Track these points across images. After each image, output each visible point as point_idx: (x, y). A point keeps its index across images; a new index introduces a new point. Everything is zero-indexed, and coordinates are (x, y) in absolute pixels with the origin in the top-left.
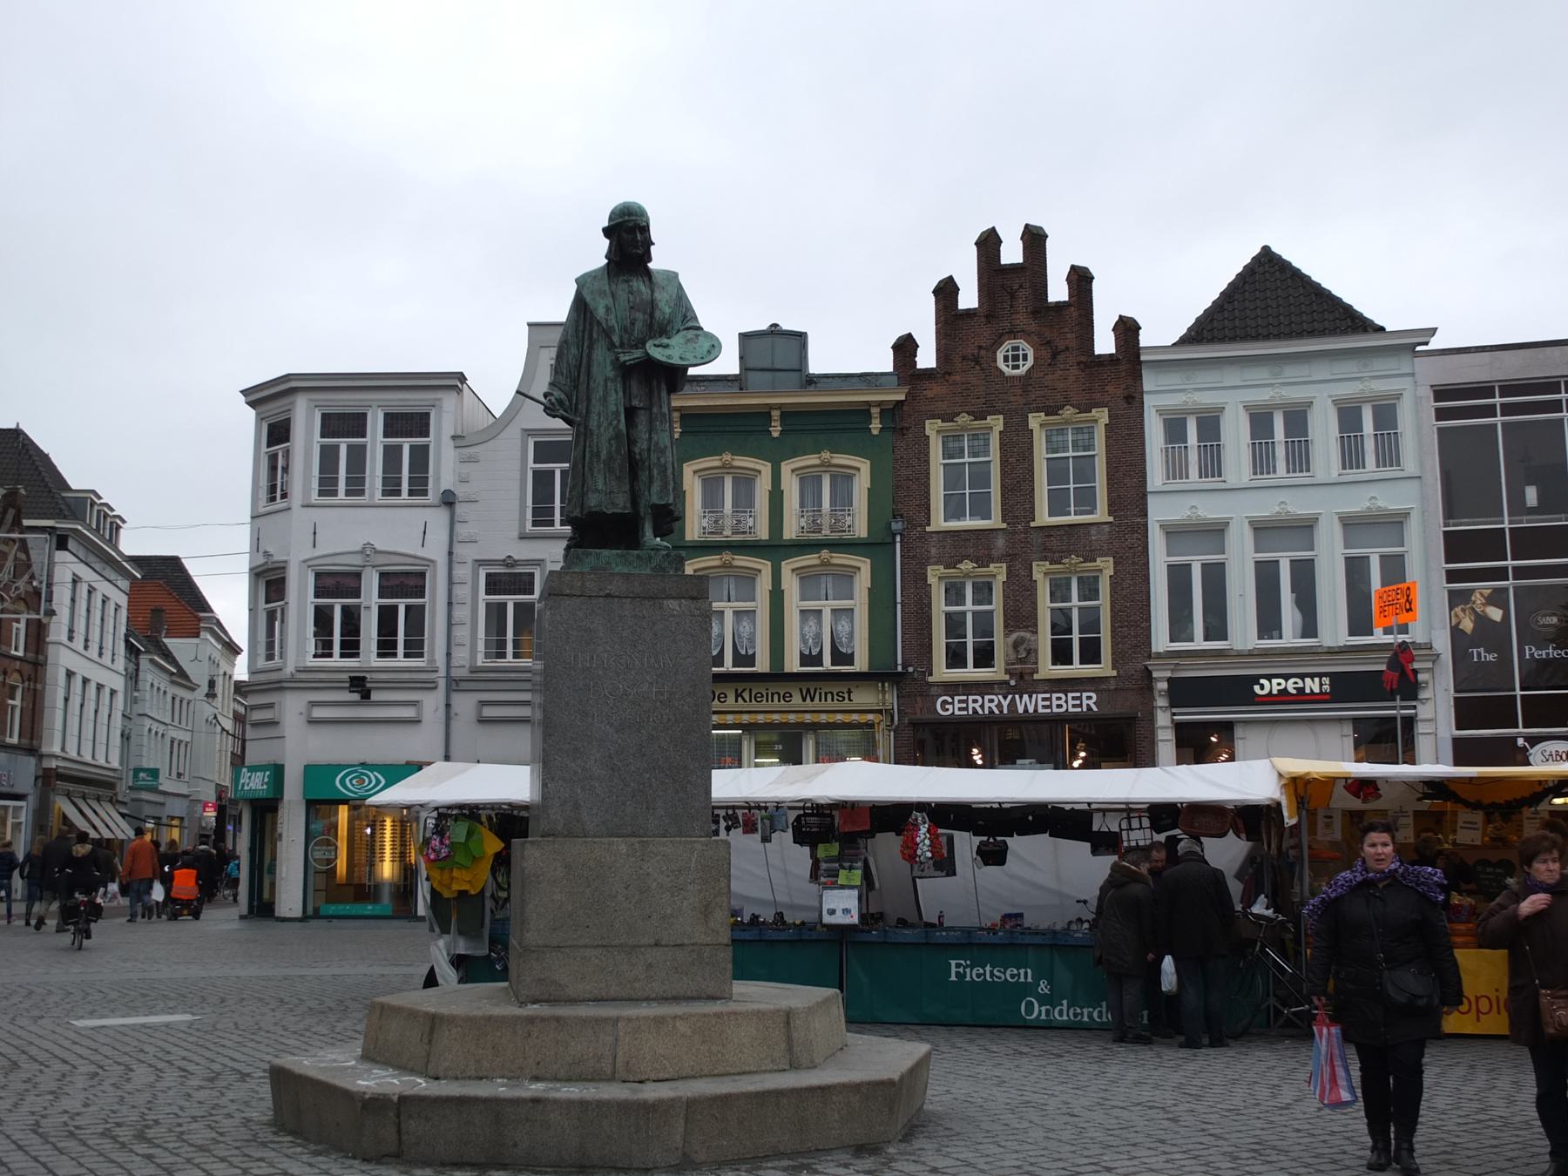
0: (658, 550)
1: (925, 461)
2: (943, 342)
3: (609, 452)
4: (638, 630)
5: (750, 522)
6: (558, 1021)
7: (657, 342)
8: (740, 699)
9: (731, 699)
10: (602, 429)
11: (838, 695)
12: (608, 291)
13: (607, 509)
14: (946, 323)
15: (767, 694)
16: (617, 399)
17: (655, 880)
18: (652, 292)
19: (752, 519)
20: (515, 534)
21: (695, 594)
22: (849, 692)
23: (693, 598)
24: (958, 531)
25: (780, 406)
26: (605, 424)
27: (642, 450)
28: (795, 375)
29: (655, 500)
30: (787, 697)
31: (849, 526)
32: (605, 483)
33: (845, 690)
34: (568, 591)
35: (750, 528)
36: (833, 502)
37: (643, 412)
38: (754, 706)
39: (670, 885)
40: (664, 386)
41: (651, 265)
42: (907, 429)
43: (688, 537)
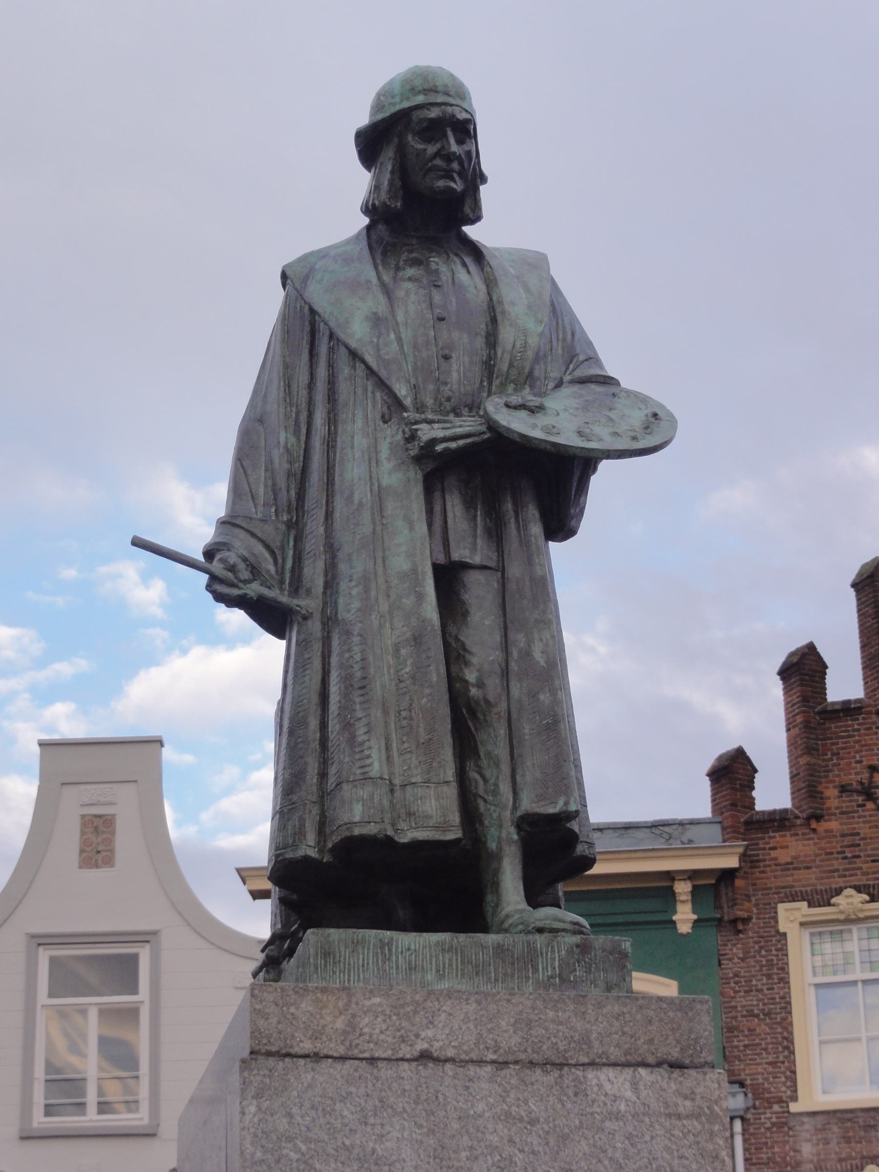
0: (554, 931)
1: (781, 980)
2: (802, 761)
7: (515, 400)
12: (374, 280)
14: (807, 726)
20: (13, 1131)
21: (675, 1054)
23: (676, 1066)
24: (852, 1111)
29: (528, 804)
34: (307, 1046)
40: (532, 512)
42: (746, 921)
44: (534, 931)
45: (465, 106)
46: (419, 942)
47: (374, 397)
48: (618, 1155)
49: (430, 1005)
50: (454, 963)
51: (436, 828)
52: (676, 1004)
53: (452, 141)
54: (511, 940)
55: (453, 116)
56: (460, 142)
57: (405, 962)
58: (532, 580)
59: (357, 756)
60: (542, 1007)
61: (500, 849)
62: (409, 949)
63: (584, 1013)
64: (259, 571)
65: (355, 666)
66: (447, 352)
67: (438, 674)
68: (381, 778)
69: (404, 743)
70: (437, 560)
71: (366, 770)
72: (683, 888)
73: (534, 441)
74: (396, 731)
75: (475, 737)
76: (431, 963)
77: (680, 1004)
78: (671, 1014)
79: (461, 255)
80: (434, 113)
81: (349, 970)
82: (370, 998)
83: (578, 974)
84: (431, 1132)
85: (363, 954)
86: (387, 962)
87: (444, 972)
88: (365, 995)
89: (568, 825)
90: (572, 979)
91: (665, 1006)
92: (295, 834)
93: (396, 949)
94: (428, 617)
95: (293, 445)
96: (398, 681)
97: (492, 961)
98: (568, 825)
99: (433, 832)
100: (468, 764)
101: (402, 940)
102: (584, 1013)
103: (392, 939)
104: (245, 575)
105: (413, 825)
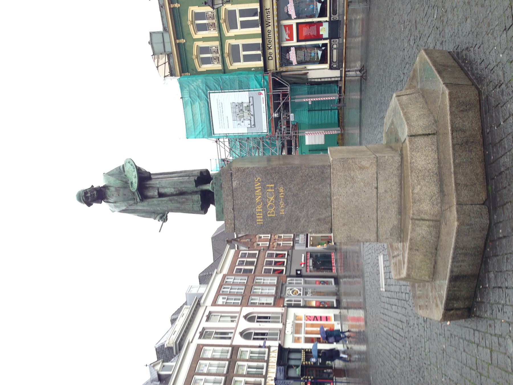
4: (246, 197)
5: (214, 48)
6: (412, 240)
8: (271, 48)
9: (271, 51)
11: (268, 14)
15: (269, 38)
17: (349, 190)
19: (213, 47)
22: (266, 9)
25: (175, 40)
28: (164, 35)
30: (269, 32)
31: (212, 13)
33: (266, 11)
34: (233, 225)
35: (216, 48)
36: (204, 19)
38: (273, 43)
39: (351, 184)
43: (221, 68)
48: (245, 183)
72: (172, 6)
80: (84, 198)
84: (244, 209)
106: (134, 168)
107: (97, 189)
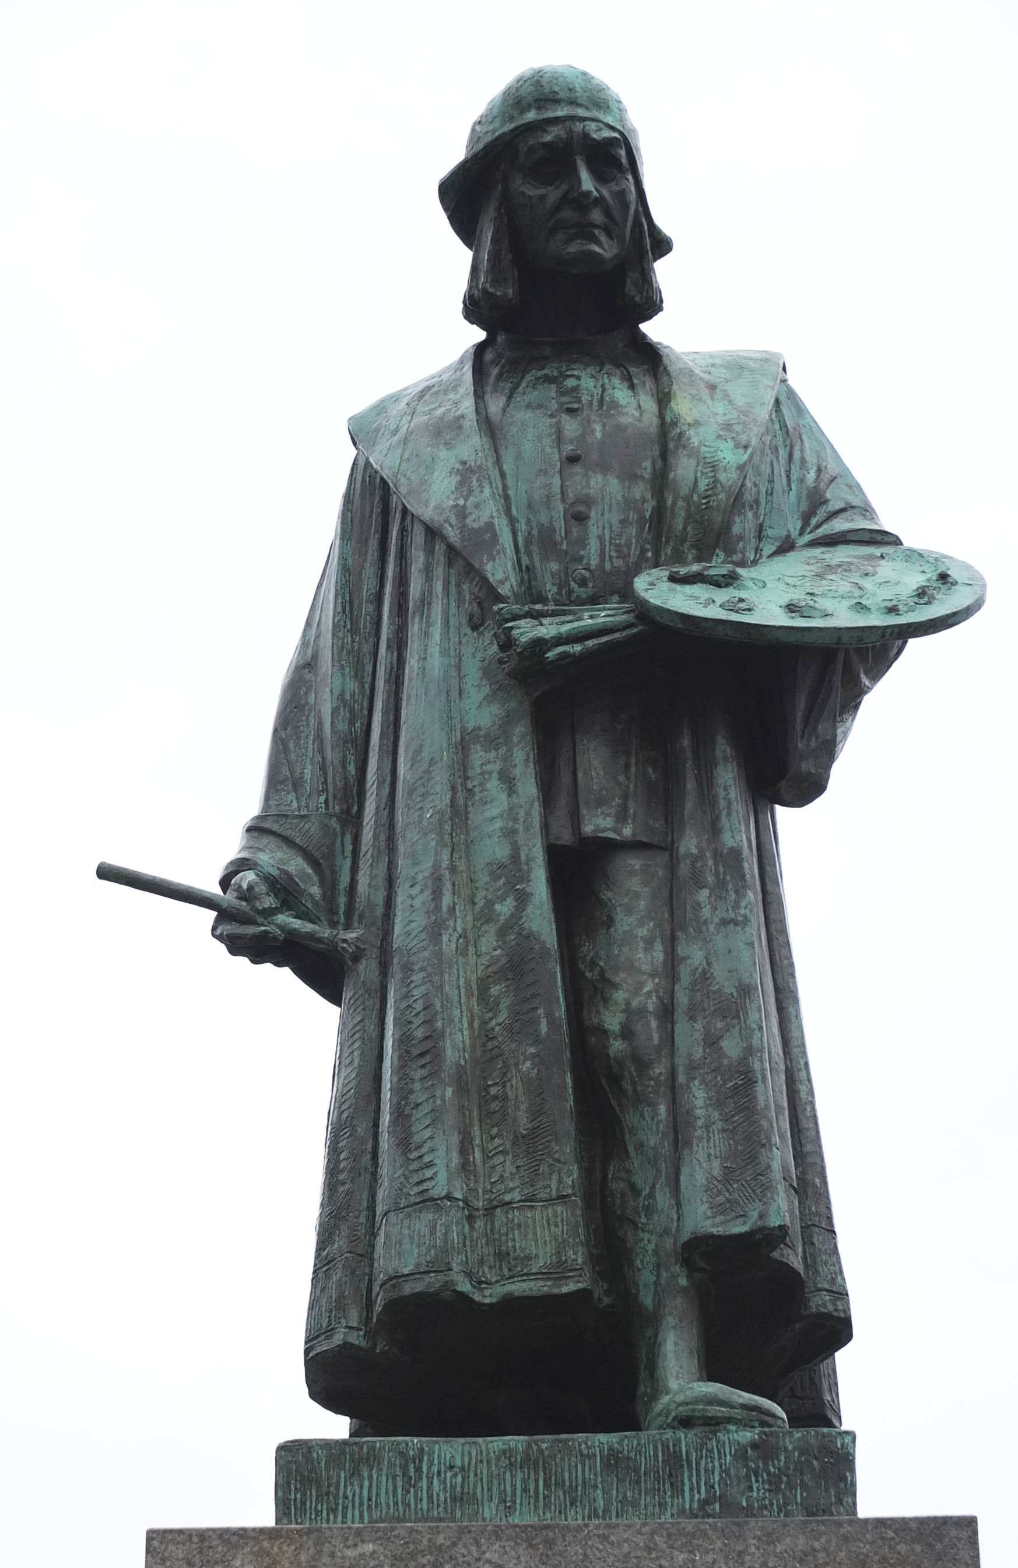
3: (484, 1035)
10: (449, 942)
13: (480, 1284)
16: (511, 813)
18: (663, 399)
26: (463, 920)
27: (633, 1015)
32: (465, 1167)
37: (635, 862)
41: (652, 329)
44: (676, 1424)
45: (609, 120)
46: (470, 1453)
47: (459, 593)
49: (464, 1551)
50: (532, 1487)
51: (543, 1275)
52: (911, 1530)
53: (585, 175)
54: (635, 1442)
55: (586, 135)
56: (601, 178)
57: (445, 1488)
58: (717, 855)
59: (414, 1166)
60: (665, 1546)
61: (659, 1304)
62: (452, 1467)
63: (740, 1554)
64: (296, 898)
65: (414, 1020)
66: (582, 508)
67: (552, 1022)
68: (449, 1197)
69: (493, 1138)
70: (558, 838)
71: (425, 1186)
73: (704, 624)
74: (481, 1121)
75: (621, 1121)
76: (490, 1489)
77: (919, 1528)
78: (902, 1548)
79: (626, 365)
81: (345, 1508)
82: (356, 1545)
83: (755, 1494)
85: (370, 1477)
86: (412, 1490)
87: (514, 1502)
88: (347, 1539)
89: (776, 1254)
90: (744, 1504)
91: (891, 1534)
92: (331, 1311)
93: (429, 1468)
94: (534, 929)
95: (353, 695)
96: (485, 1039)
97: (599, 1480)
98: (776, 1254)
99: (541, 1283)
100: (612, 1168)
101: (440, 1452)
102: (740, 1554)
103: (421, 1450)
104: (269, 902)
105: (506, 1271)
106: (893, 610)
107: (632, 276)
